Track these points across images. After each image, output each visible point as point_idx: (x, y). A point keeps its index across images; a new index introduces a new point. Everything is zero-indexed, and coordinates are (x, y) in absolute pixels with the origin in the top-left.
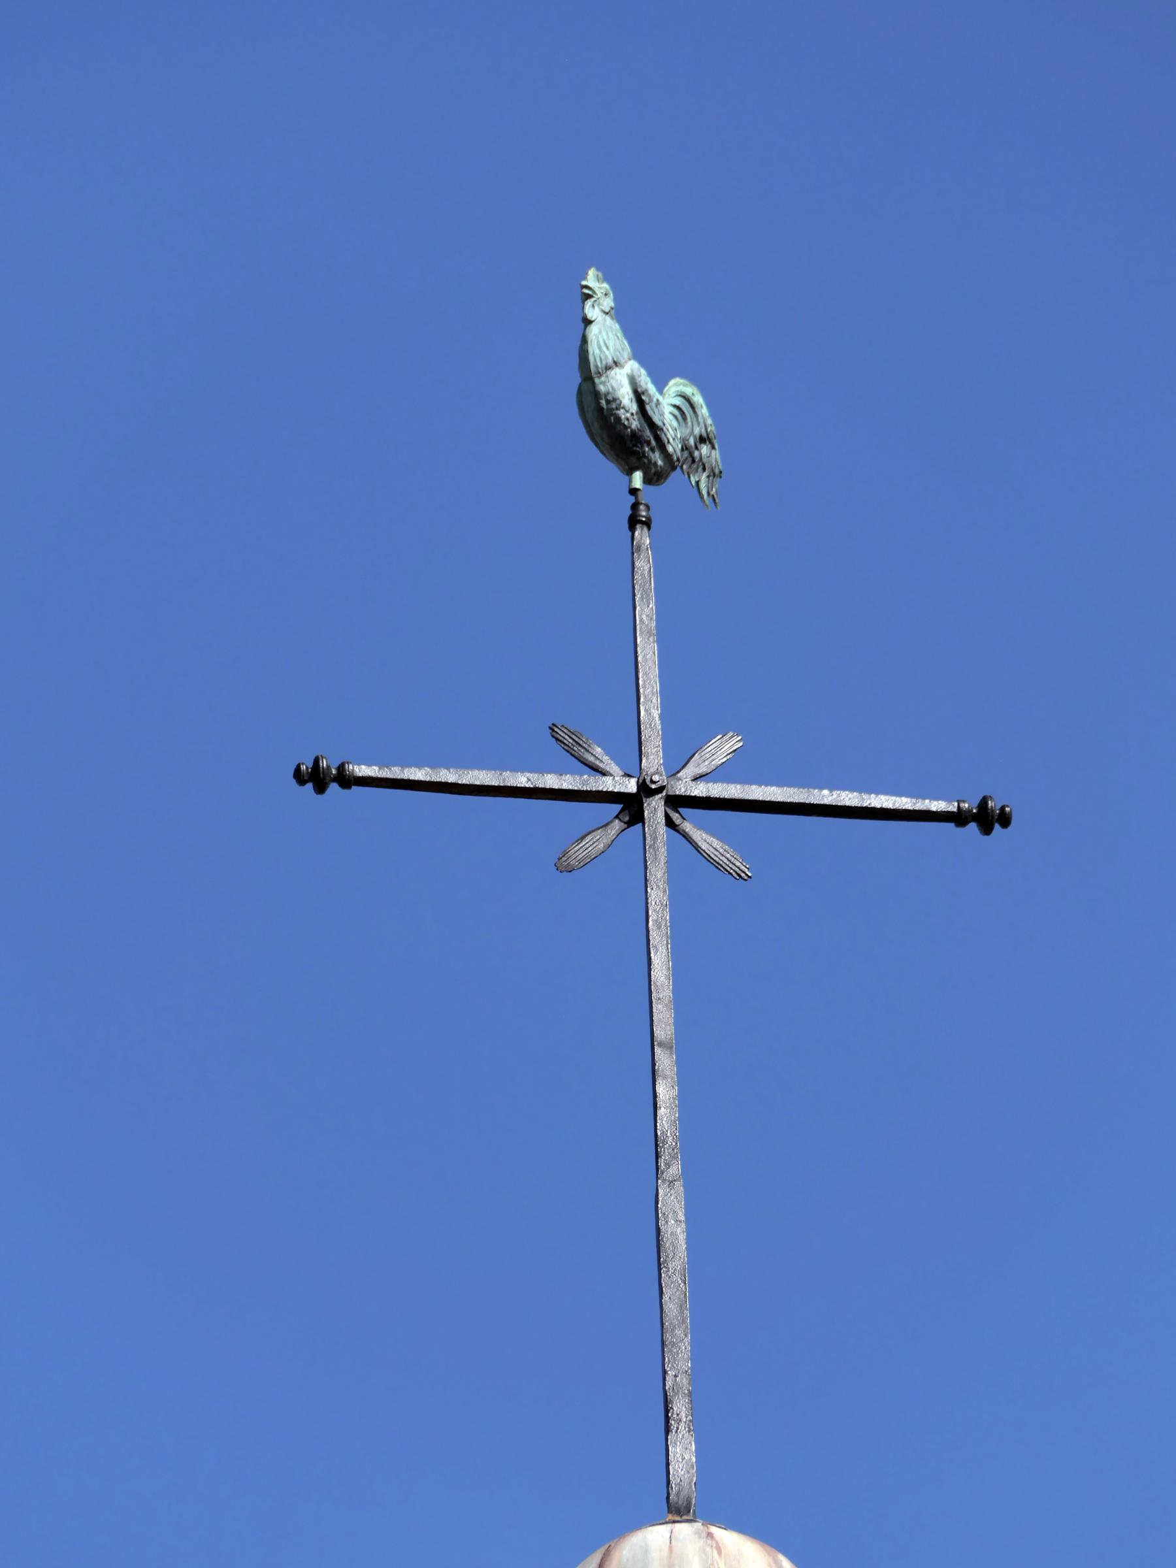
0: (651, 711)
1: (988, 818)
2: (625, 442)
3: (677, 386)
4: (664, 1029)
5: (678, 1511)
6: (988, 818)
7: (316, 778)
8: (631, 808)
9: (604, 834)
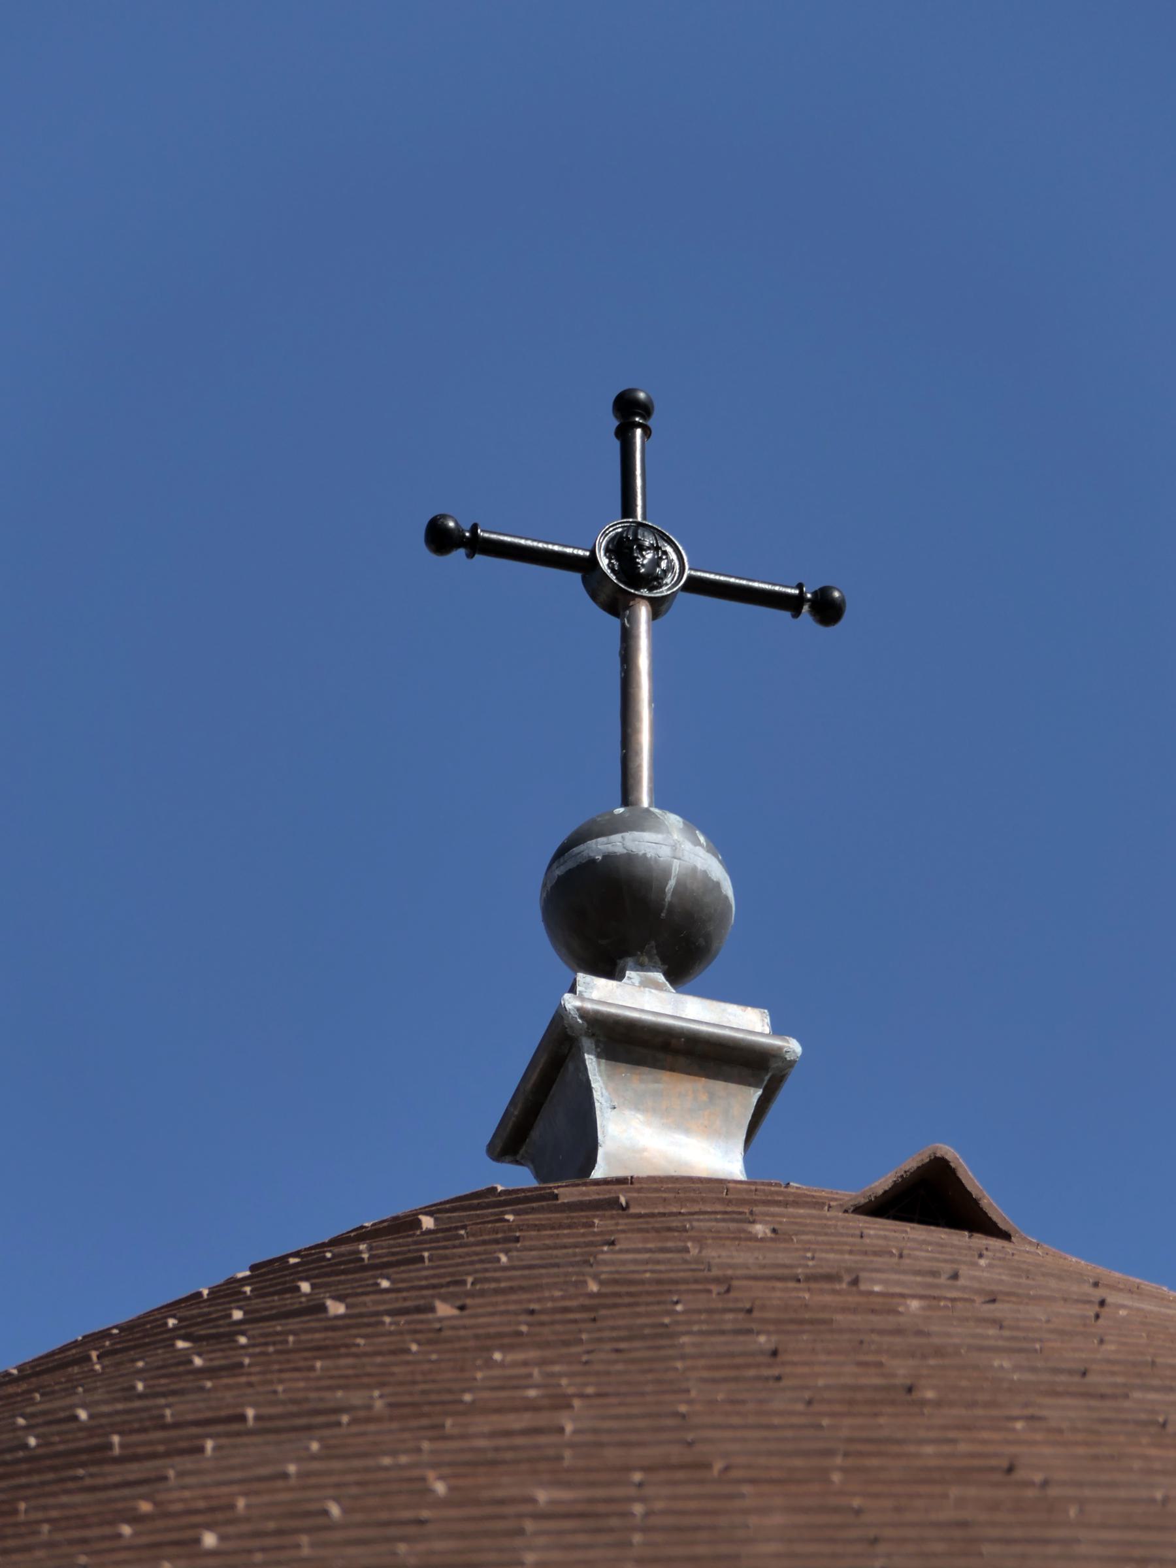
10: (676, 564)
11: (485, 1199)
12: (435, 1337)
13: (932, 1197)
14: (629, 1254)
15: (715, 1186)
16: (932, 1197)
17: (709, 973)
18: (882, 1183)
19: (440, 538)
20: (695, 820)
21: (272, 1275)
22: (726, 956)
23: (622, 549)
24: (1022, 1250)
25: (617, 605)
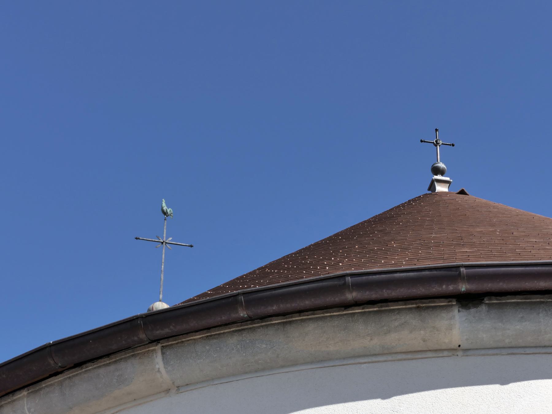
0: (165, 235)
1: (191, 246)
2: (165, 213)
3: (170, 209)
4: (163, 261)
5: (160, 301)
6: (191, 246)
7: (137, 238)
8: (162, 243)
9: (160, 245)
10: (441, 142)
11: (426, 194)
12: (421, 206)
13: (462, 192)
14: (437, 198)
15: (445, 192)
16: (462, 192)
17: (445, 175)
18: (458, 191)
19: (422, 141)
20: (443, 163)
21: (409, 201)
22: (446, 173)
23: (436, 141)
24: (470, 196)
25: (436, 146)
